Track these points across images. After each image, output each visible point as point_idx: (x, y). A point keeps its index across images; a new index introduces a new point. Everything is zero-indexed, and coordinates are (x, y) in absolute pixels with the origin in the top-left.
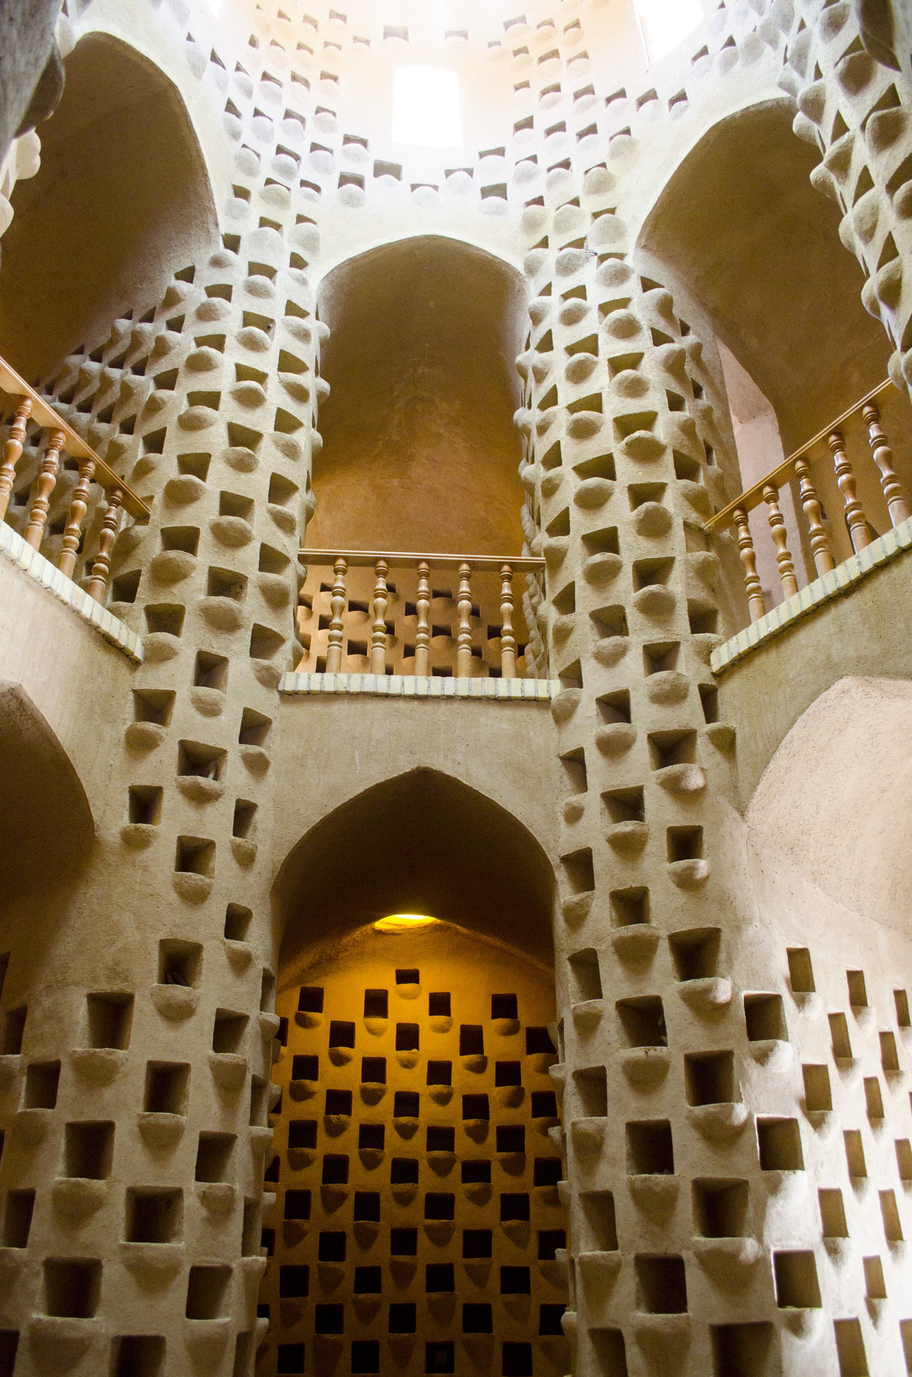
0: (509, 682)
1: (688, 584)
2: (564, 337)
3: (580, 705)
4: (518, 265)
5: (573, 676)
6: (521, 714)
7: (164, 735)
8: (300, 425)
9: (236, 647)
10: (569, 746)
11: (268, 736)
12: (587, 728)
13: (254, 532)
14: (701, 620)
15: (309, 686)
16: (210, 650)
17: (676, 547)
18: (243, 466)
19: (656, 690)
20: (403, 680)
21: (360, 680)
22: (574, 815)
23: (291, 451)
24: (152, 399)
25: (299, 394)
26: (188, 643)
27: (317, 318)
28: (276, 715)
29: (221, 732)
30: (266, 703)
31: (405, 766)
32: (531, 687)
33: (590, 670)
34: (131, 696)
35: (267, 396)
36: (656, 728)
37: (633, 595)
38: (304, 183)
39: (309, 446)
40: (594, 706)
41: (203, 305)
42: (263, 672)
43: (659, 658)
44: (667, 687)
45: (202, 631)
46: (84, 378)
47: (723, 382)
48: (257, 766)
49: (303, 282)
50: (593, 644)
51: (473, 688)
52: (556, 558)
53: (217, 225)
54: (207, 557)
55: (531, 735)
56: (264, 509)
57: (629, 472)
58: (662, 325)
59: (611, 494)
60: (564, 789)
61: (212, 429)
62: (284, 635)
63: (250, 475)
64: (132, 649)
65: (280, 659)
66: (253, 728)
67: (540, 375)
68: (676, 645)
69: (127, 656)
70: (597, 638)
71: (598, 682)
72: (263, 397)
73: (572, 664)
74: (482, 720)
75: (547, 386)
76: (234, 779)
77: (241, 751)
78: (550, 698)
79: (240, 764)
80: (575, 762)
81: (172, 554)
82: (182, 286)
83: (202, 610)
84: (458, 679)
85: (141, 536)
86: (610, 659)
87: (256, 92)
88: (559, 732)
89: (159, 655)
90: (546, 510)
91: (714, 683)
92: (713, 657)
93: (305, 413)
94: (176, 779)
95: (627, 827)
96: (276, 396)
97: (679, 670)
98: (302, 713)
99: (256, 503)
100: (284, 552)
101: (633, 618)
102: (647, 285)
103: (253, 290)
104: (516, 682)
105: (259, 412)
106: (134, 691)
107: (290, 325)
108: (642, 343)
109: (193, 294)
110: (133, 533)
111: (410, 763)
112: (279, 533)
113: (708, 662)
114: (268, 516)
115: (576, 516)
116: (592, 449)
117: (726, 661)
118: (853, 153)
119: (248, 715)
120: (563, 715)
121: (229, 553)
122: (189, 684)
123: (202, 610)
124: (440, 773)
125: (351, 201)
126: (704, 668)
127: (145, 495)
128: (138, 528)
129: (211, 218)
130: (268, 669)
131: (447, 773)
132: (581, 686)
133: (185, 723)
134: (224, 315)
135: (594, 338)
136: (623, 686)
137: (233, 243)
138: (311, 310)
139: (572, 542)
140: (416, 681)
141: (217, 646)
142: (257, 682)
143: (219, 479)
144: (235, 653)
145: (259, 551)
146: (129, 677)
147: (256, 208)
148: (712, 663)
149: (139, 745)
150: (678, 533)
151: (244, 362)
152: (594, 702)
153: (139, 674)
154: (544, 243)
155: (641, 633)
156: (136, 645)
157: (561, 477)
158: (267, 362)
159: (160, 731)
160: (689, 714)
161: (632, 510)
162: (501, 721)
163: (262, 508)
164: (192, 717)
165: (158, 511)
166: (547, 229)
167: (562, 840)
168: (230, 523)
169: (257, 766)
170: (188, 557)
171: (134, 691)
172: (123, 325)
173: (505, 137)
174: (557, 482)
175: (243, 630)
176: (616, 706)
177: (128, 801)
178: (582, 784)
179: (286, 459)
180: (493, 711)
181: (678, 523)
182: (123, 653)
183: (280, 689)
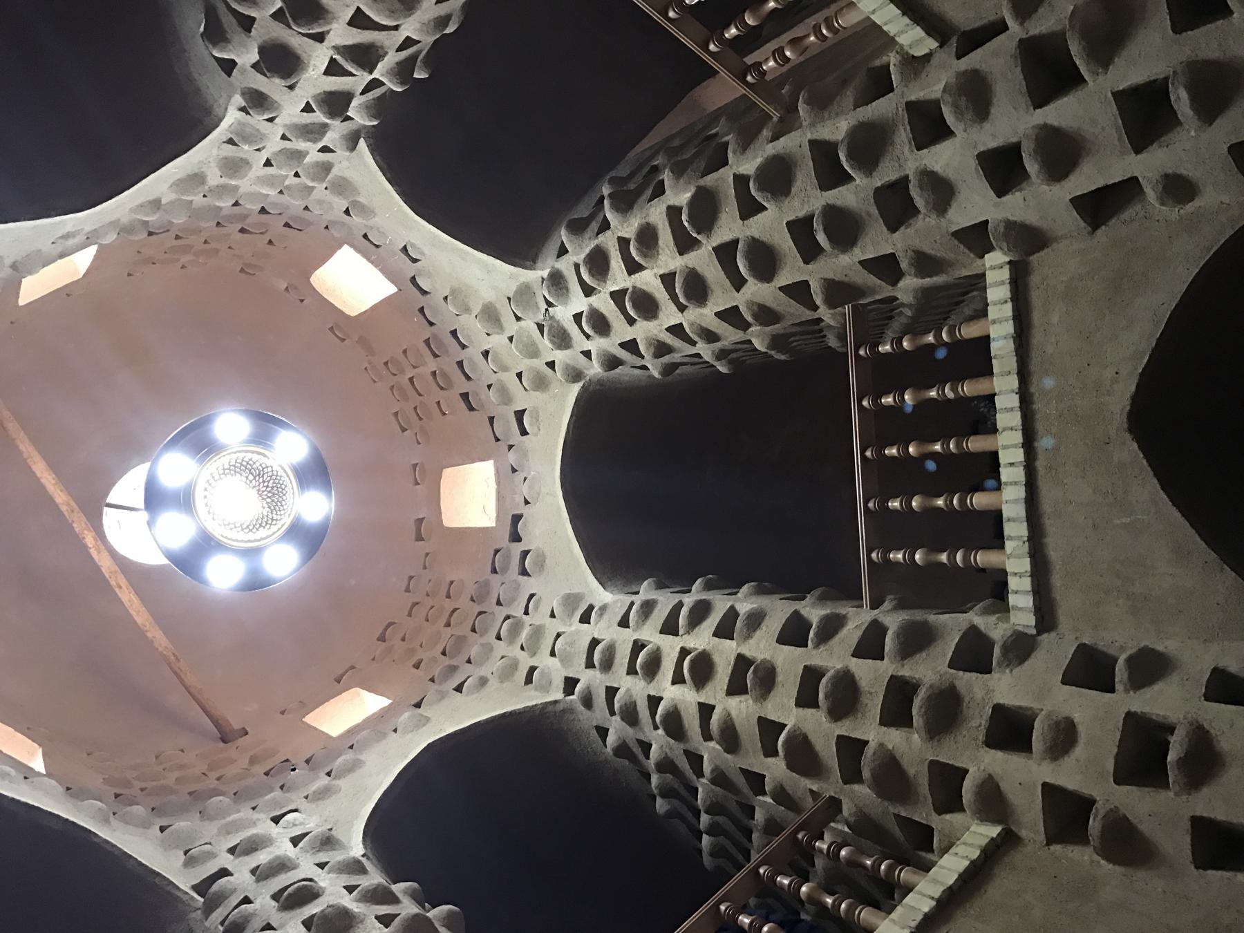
0: (994, 322)
1: (837, 114)
2: (621, 331)
3: (1011, 218)
4: (576, 389)
5: (977, 238)
6: (1037, 298)
7: (1109, 806)
8: (732, 608)
9: (979, 693)
10: (1072, 221)
11: (1105, 649)
12: (1043, 201)
13: (839, 666)
14: (880, 84)
15: (1026, 592)
16: (983, 730)
17: (798, 143)
18: (768, 678)
19: (969, 115)
20: (1005, 466)
21: (1011, 524)
22: (1178, 188)
23: (755, 620)
24: (714, 781)
25: (700, 612)
26: (980, 762)
27: (637, 593)
28: (1073, 637)
29: (1098, 716)
30: (1055, 652)
31: (1129, 451)
32: (998, 293)
33: (962, 215)
34: (1056, 848)
35: (701, 648)
36: (1024, 101)
37: (858, 181)
38: (526, 613)
39: (754, 598)
40: (1008, 198)
41: (622, 719)
42: (1011, 655)
43: (929, 126)
44: (963, 102)
45: (959, 738)
46: (716, 852)
47: (650, 148)
48: (1150, 667)
49: (604, 608)
50: (927, 219)
51: (1007, 369)
52: (838, 292)
53: (556, 702)
54: (869, 729)
55: (1065, 279)
56: (814, 652)
57: (729, 227)
58: (595, 226)
59: (753, 238)
60: (1142, 213)
61: (734, 714)
62: (965, 626)
63: (778, 670)
64: (987, 840)
65: (997, 630)
66: (1091, 670)
67: (661, 349)
68: (910, 106)
69: (998, 847)
70: (921, 217)
71: (977, 203)
72: (700, 654)
73: (961, 242)
74: (1050, 349)
75: (669, 339)
76: (1167, 701)
77: (1127, 691)
78: (1010, 262)
79: (1148, 692)
80: (1098, 207)
81: (866, 773)
82: (611, 739)
83: (932, 738)
84: (997, 391)
85: (854, 809)
86: (942, 191)
87: (454, 662)
88: (1056, 240)
89: (993, 802)
90: (792, 315)
91: (954, 40)
92: (919, 52)
93: (721, 603)
94: (1176, 794)
95: (1181, 99)
96: (701, 639)
97: (938, 95)
98: (1068, 601)
99: (808, 663)
100: (864, 628)
101: (886, 174)
102: (563, 251)
103: (607, 665)
104: (993, 312)
105: (717, 658)
106: (1049, 843)
107: (637, 622)
108: (609, 241)
109: (617, 729)
110: (852, 819)
111: (1124, 444)
112: (843, 633)
113: (928, 57)
114: (822, 648)
115: (786, 277)
116: (713, 273)
117: (918, 32)
118: (347, 43)
119: (1071, 678)
120: (1028, 241)
121: (864, 699)
122: (1030, 762)
123: (932, 738)
124: (1135, 399)
125: (541, 563)
126: (935, 61)
127: (810, 799)
128: (846, 812)
129: (550, 708)
130: (1006, 649)
131: (1133, 388)
132: (987, 222)
133: (1087, 771)
134: (631, 696)
135: (613, 295)
136: (973, 163)
137: (570, 684)
138: (675, 599)
139: (814, 275)
140: (1005, 447)
141: (978, 720)
142: (1026, 663)
143: (782, 706)
144: (986, 694)
145: (860, 660)
146: (1029, 849)
147: (545, 662)
148: (927, 51)
149: (1125, 844)
150: (785, 144)
151: (670, 676)
152: (1005, 199)
153: (1024, 833)
154: (551, 365)
155: (906, 160)
156: (978, 834)
157: (750, 304)
158: (670, 647)
159: (1102, 813)
160: (995, 59)
161: (765, 208)
162: (1050, 321)
163: (814, 656)
164: (1077, 761)
165: (825, 786)
166: (539, 364)
167: (1226, 199)
168: (827, 697)
169: (1150, 667)
170: (869, 751)
171: (1049, 843)
172: (661, 805)
173: (481, 418)
174: (756, 308)
175: (957, 683)
176: (1003, 169)
177: (1219, 873)
178: (1128, 190)
179: (763, 626)
180: (1037, 337)
181: (771, 149)
182: (992, 855)
183: (1034, 632)
